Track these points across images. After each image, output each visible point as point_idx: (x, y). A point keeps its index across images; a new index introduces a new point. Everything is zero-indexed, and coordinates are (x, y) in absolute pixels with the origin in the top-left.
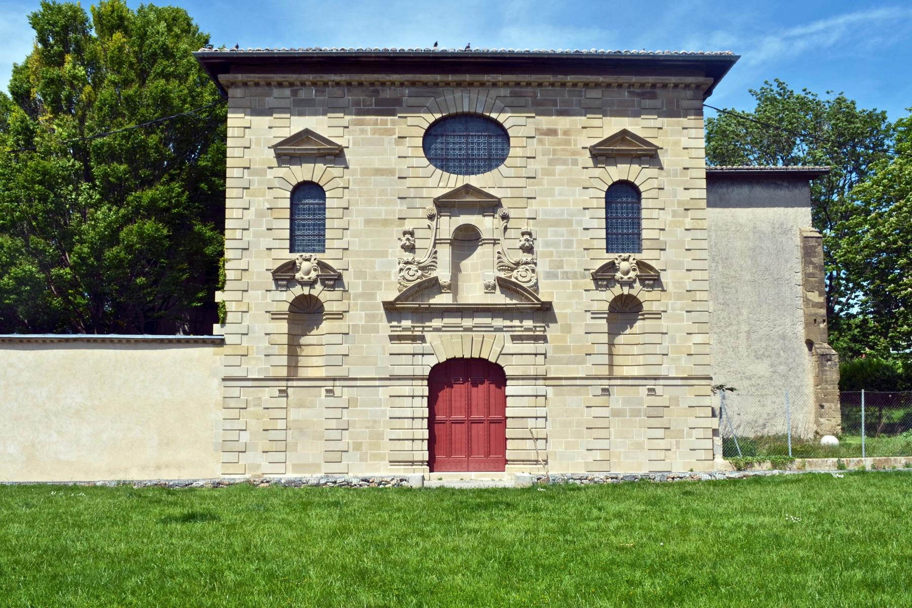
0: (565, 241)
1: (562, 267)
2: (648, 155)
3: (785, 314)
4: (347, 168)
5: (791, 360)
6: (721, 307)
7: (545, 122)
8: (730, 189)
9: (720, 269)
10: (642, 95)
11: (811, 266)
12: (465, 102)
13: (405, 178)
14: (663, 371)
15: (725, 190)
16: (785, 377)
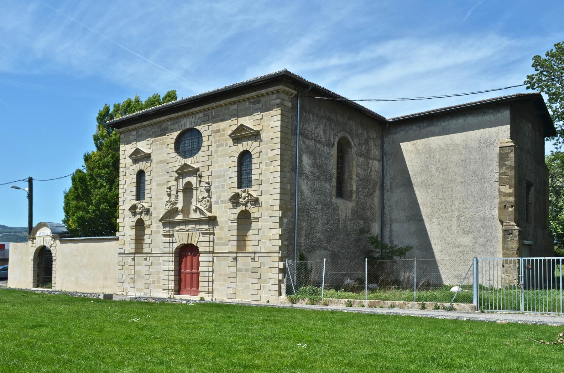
0: (222, 185)
1: (220, 198)
2: (256, 136)
3: (486, 202)
4: (261, 141)
5: (488, 234)
6: (441, 201)
7: (215, 126)
8: (450, 122)
9: (441, 176)
10: (254, 103)
11: (504, 167)
12: (187, 123)
13: (19, 189)
14: (258, 249)
15: (447, 123)
16: (484, 245)
